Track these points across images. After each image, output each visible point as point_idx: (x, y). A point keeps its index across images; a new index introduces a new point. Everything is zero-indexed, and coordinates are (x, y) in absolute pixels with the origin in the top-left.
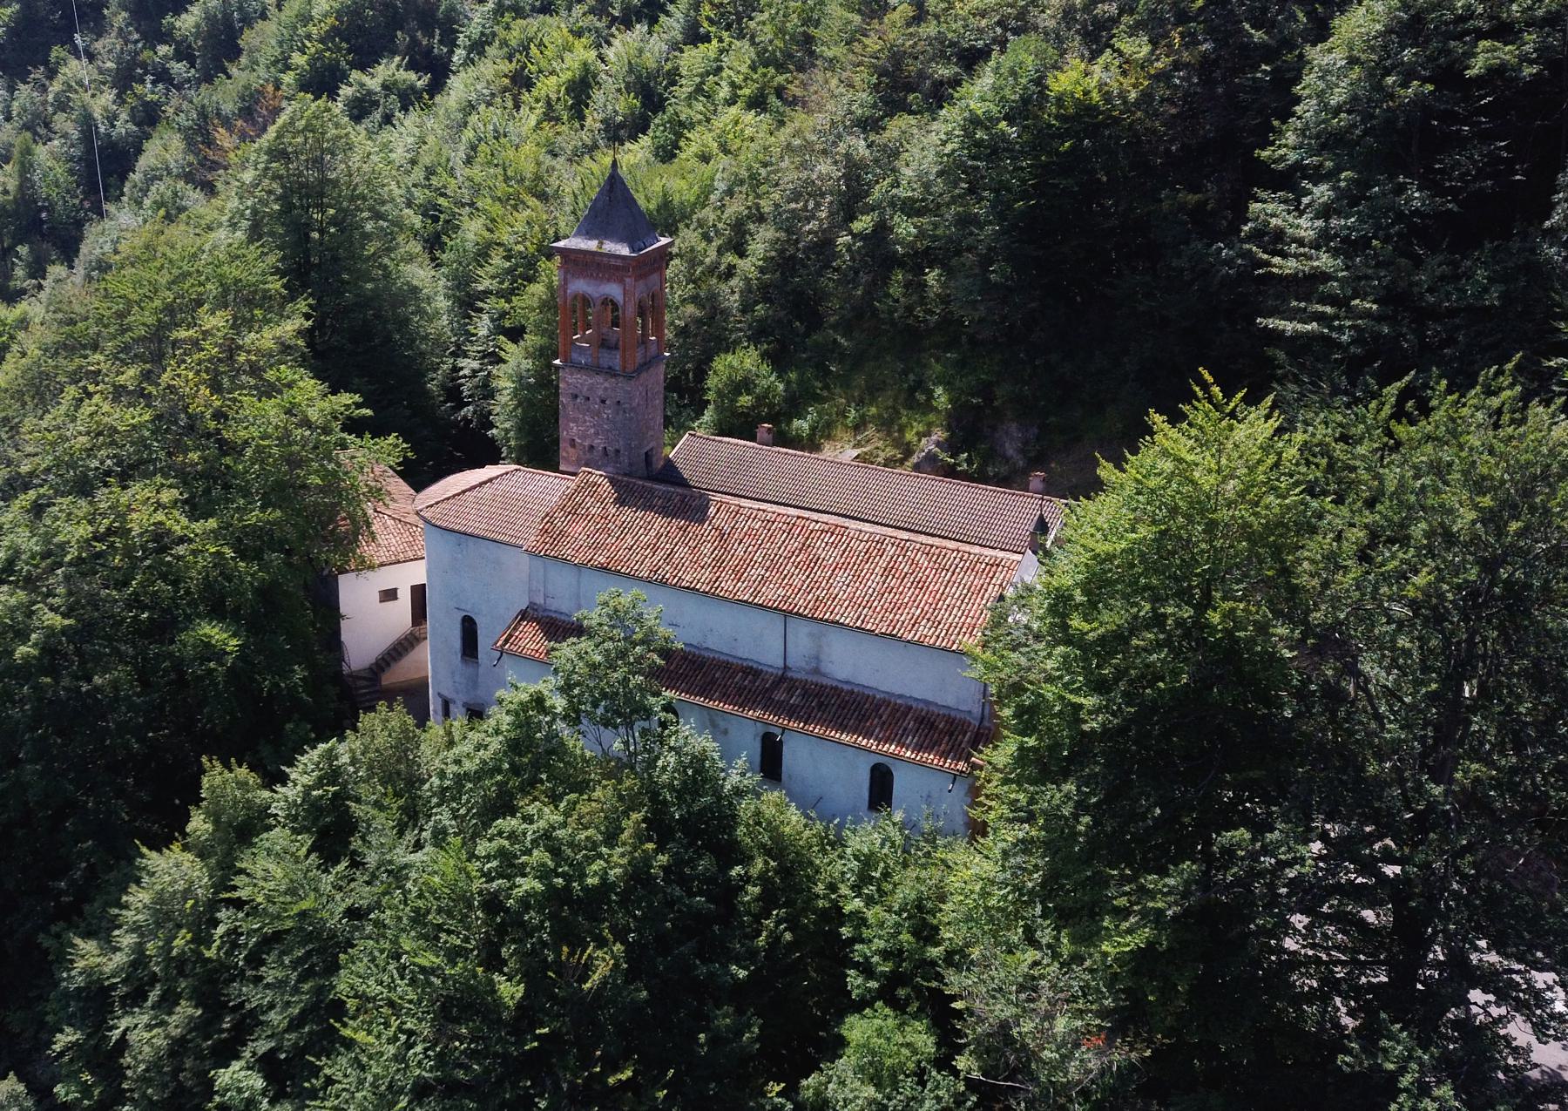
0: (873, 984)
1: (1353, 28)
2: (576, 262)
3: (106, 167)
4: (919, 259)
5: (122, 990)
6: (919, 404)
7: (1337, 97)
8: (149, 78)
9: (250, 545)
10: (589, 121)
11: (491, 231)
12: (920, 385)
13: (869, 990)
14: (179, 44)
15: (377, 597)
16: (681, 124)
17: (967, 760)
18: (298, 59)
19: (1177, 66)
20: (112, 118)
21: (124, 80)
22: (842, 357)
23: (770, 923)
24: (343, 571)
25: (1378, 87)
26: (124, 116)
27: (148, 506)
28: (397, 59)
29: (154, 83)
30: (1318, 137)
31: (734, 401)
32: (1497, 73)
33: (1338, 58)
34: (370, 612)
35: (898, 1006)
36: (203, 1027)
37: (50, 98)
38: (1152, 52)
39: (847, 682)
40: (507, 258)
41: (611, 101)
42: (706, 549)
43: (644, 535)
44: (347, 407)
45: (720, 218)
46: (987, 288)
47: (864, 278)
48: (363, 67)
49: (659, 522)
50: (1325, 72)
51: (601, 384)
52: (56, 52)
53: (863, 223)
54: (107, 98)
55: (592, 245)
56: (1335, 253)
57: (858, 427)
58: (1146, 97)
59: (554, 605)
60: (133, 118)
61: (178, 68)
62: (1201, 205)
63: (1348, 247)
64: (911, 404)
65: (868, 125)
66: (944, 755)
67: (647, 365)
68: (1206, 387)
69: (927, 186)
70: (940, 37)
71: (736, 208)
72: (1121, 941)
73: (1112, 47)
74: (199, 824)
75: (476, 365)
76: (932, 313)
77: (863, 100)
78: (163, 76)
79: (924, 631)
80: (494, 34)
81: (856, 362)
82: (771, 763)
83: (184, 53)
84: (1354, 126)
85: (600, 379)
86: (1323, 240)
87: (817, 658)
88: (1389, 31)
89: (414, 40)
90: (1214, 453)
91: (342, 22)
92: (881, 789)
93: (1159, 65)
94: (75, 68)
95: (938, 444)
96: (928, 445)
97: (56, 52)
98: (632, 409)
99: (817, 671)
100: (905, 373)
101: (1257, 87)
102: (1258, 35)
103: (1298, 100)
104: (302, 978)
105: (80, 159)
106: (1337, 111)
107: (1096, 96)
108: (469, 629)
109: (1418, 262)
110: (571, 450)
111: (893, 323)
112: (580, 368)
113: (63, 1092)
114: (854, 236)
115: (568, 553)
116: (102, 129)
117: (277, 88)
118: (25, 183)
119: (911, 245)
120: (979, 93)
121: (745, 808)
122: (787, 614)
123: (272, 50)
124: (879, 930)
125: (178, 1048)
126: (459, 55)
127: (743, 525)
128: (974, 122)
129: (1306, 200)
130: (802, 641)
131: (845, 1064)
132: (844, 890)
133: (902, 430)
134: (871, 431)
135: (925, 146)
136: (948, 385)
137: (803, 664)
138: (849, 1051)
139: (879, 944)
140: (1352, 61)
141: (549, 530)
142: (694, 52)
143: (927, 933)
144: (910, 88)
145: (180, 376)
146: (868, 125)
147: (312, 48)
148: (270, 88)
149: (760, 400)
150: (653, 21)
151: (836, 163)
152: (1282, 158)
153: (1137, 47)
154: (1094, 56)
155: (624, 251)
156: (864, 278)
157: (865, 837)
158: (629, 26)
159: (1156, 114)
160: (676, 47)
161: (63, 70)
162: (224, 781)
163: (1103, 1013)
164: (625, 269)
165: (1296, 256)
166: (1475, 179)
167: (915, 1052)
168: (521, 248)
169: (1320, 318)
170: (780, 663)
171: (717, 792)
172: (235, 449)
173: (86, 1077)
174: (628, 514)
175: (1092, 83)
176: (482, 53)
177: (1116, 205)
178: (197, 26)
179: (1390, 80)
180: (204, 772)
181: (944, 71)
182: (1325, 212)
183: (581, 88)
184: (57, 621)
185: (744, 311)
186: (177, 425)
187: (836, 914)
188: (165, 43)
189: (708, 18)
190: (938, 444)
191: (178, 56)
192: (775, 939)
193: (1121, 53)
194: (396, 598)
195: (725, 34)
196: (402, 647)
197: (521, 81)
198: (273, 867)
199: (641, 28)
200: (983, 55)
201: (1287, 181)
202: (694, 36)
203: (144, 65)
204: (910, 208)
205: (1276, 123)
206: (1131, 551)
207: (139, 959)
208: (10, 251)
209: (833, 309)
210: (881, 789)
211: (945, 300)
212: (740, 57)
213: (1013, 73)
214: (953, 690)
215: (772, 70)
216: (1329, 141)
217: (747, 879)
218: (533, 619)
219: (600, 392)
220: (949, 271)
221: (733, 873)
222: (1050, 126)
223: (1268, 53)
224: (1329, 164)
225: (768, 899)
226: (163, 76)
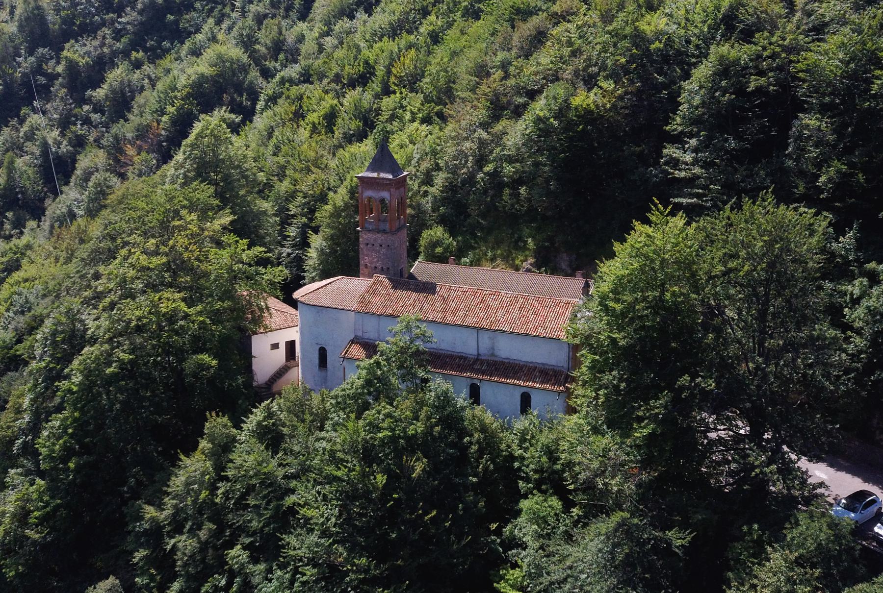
0: (530, 485)
3: (57, 170)
4: (517, 182)
5: (168, 528)
6: (521, 248)
7: (697, 101)
8: (79, 122)
9: (216, 316)
10: (336, 133)
11: (295, 185)
12: (520, 239)
13: (529, 488)
14: (95, 105)
15: (270, 347)
16: (387, 132)
17: (564, 386)
18: (170, 109)
19: (626, 93)
20: (58, 144)
21: (64, 124)
22: (482, 229)
23: (483, 461)
24: (255, 333)
25: (713, 97)
26: (65, 143)
27: (171, 300)
28: (224, 108)
29: (82, 125)
30: (690, 119)
31: (433, 250)
32: (759, 90)
33: (695, 86)
34: (266, 354)
35: (543, 492)
36: (217, 534)
37: (21, 134)
38: (615, 87)
40: (305, 197)
41: (346, 123)
42: (438, 304)
43: (408, 304)
44: (261, 252)
45: (418, 171)
46: (549, 193)
47: (491, 192)
48: (206, 112)
49: (414, 295)
50: (690, 92)
51: (380, 238)
52: (24, 111)
53: (489, 168)
54: (56, 133)
55: (375, 175)
56: (702, 167)
57: (493, 260)
58: (614, 106)
59: (366, 336)
60: (70, 143)
61: (95, 117)
62: (642, 152)
63: (706, 165)
64: (518, 248)
65: (485, 126)
66: (554, 385)
67: (399, 229)
68: (656, 205)
69: (518, 149)
70: (517, 86)
71: (426, 165)
72: (641, 432)
73: (597, 85)
74: (204, 444)
75: (289, 250)
76: (523, 206)
77: (482, 113)
78: (87, 121)
79: (540, 331)
80: (282, 93)
81: (488, 231)
82: (475, 394)
83: (98, 108)
84: (704, 114)
85: (379, 235)
86: (695, 162)
87: (493, 349)
88: (715, 74)
89: (232, 98)
90: (660, 235)
91: (193, 90)
92: (526, 403)
93: (619, 92)
94: (35, 119)
95: (531, 265)
96: (526, 265)
97: (24, 111)
98: (395, 248)
99: (493, 355)
100: (513, 234)
101: (660, 101)
102: (660, 79)
103: (680, 104)
104: (268, 504)
105: (40, 166)
106: (697, 108)
107: (593, 107)
108: (323, 354)
109: (736, 170)
111: (505, 212)
112: (369, 231)
113: (140, 581)
114: (485, 174)
115: (374, 310)
116: (54, 149)
117: (159, 124)
118: (10, 178)
119: (511, 177)
120: (539, 107)
121: (468, 413)
123: (153, 104)
124: (532, 459)
125: (204, 546)
126: (260, 106)
127: (453, 294)
128: (539, 120)
129: (687, 146)
130: (485, 341)
131: (522, 520)
132: (515, 447)
133: (513, 260)
134: (499, 261)
135: (516, 133)
136: (534, 238)
137: (486, 352)
138: (523, 513)
139: (532, 466)
140: (701, 87)
141: (362, 300)
142: (388, 99)
143: (554, 459)
144: (503, 108)
145: (180, 241)
146: (485, 126)
147: (178, 103)
148: (155, 124)
149: (446, 250)
150: (365, 85)
151: (473, 142)
152: (675, 129)
153: (609, 85)
154: (589, 90)
155: (391, 177)
156: (491, 192)
157: (521, 423)
158: (354, 88)
159: (619, 113)
160: (377, 96)
161: (29, 119)
162: (217, 424)
163: (638, 462)
164: (390, 184)
165: (685, 170)
166: (756, 134)
167: (553, 509)
168: (311, 192)
169: (698, 196)
170: (476, 353)
171: (455, 406)
172: (206, 275)
173: (153, 571)
174: (399, 293)
175: (590, 101)
176: (275, 103)
177: (604, 154)
178: (106, 95)
179: (717, 94)
180: (206, 420)
181: (520, 100)
182: (696, 150)
183: (331, 118)
184: (125, 357)
185: (434, 211)
186: (177, 266)
187: (512, 458)
188: (87, 104)
189: (394, 83)
190: (531, 265)
191: (95, 111)
192: (486, 469)
193: (601, 88)
194: (278, 348)
195: (403, 90)
196: (281, 373)
197: (299, 115)
198: (248, 456)
199: (359, 89)
200: (540, 91)
201: (678, 139)
202: (387, 91)
203: (76, 116)
204: (510, 160)
205: (671, 115)
206: (631, 274)
207: (178, 511)
208: (2, 214)
209: (473, 210)
210: (526, 403)
211: (529, 200)
212: (415, 101)
213: (555, 98)
214: (557, 358)
215: (433, 104)
216: (696, 121)
217: (471, 443)
219: (379, 241)
220: (530, 188)
221: (465, 440)
222: (573, 120)
223: (665, 86)
224: (695, 130)
225: (481, 452)
226: (87, 121)
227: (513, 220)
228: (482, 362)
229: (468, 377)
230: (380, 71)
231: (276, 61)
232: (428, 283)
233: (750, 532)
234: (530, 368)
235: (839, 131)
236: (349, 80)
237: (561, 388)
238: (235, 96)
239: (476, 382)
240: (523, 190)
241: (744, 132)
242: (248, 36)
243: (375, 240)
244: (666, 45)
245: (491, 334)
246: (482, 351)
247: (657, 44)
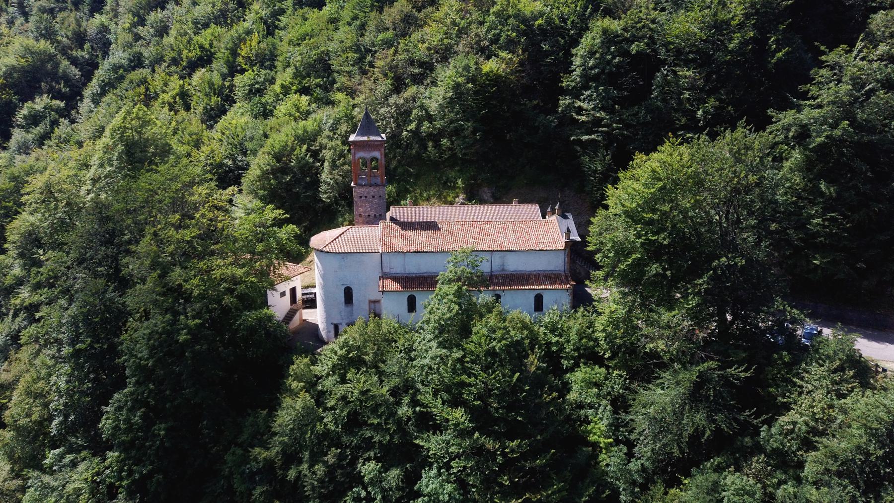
2: (359, 146)
51: (373, 191)
55: (365, 138)
57: (428, 199)
59: (393, 271)
66: (560, 284)
81: (417, 177)
87: (503, 265)
89: (51, 86)
99: (503, 270)
108: (348, 294)
112: (362, 186)
122: (492, 251)
130: (497, 260)
133: (445, 198)
135: (434, 97)
183: (184, 96)
184: (192, 323)
218: (387, 278)
227: (436, 166)
228: (497, 277)
230: (222, 53)
231: (83, 49)
233: (781, 358)
234: (535, 276)
235: (707, 79)
236: (188, 63)
238: (54, 84)
239: (498, 292)
240: (444, 141)
241: (622, 84)
242: (46, 28)
243: (368, 193)
244: (546, 21)
245: (502, 254)
247: (540, 21)
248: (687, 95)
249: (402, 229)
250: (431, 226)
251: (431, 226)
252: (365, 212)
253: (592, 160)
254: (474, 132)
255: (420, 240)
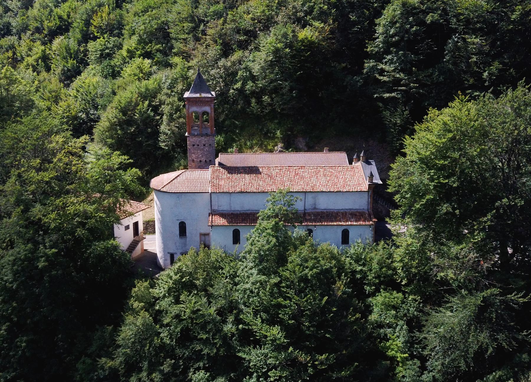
1: (391, 12)
39: (325, 209)
49: (247, 176)
51: (204, 140)
55: (198, 95)
59: (221, 209)
81: (242, 128)
87: (315, 204)
92: (345, 238)
95: (281, 148)
99: (315, 208)
108: (183, 227)
110: (193, 163)
112: (195, 136)
120: (268, 41)
122: (305, 192)
130: (310, 199)
133: (266, 146)
135: (257, 60)
137: (310, 207)
170: (303, 209)
194: (129, 228)
210: (345, 238)
219: (203, 142)
228: (309, 214)
229: (306, 225)
232: (252, 167)
235: (493, 45)
237: (371, 223)
239: (310, 228)
240: (266, 98)
243: (200, 142)
245: (313, 195)
246: (307, 207)
248: (474, 59)
249: (229, 173)
250: (253, 170)
251: (253, 170)
252: (197, 158)
253: (392, 114)
254: (291, 90)
255: (244, 182)
